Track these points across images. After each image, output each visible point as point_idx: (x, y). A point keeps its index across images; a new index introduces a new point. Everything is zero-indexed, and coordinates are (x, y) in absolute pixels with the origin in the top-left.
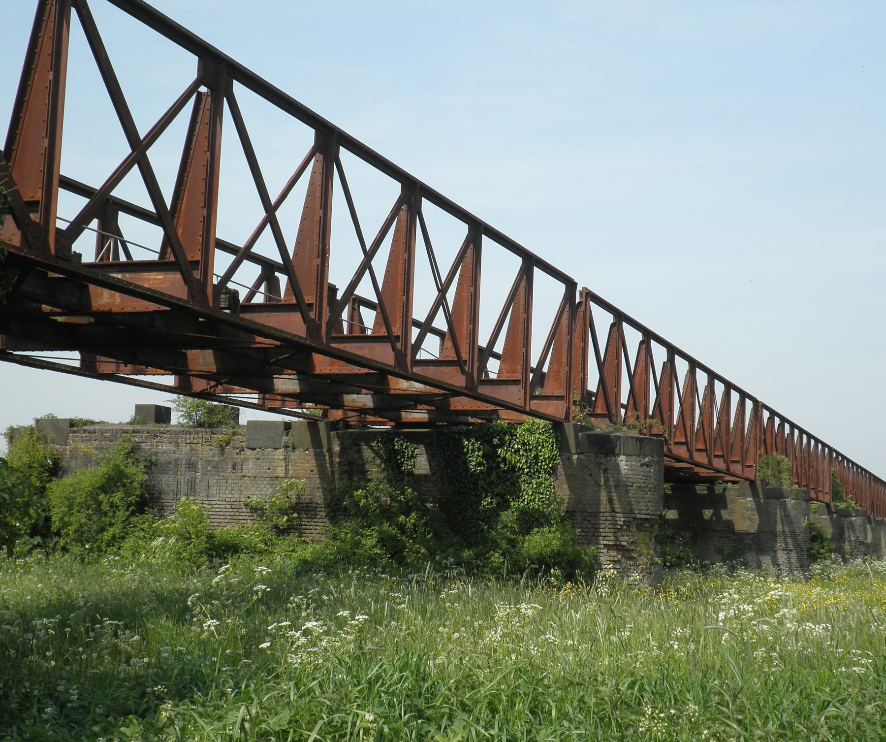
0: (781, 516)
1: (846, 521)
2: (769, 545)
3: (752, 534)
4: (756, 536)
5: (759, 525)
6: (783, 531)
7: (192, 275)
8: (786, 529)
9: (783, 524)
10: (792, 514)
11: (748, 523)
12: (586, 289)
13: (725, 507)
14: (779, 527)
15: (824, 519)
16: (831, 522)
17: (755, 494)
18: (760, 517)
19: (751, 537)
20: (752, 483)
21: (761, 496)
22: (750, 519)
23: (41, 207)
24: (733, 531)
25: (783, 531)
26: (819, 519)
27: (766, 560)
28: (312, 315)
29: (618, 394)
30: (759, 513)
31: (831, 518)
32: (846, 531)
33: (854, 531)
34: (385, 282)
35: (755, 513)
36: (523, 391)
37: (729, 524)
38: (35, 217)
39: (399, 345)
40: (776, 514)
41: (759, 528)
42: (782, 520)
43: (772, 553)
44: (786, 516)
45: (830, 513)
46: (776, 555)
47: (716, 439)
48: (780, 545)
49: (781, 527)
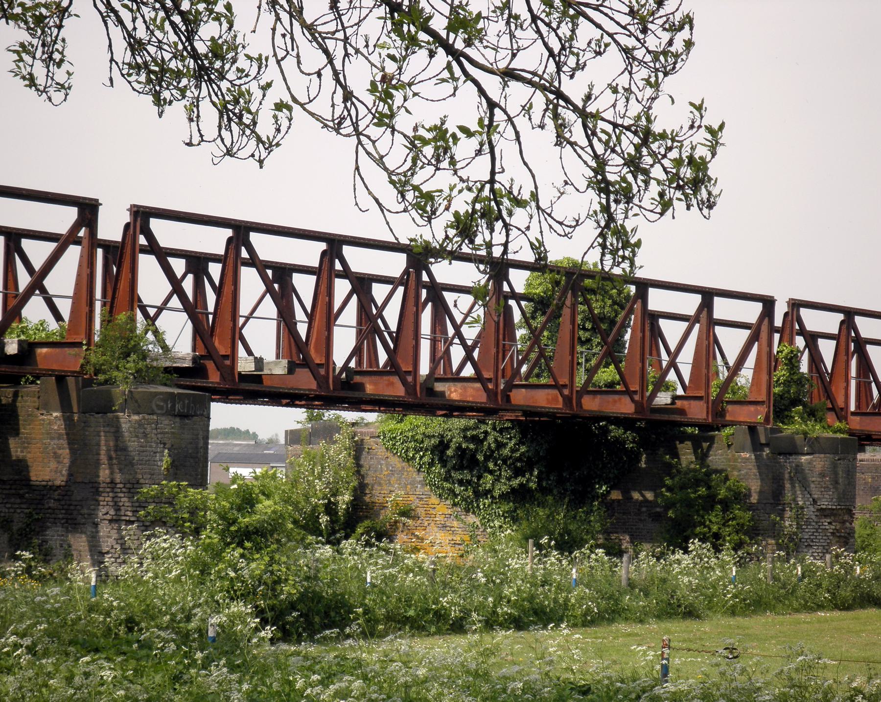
0: (108, 450)
1: (788, 464)
2: (85, 511)
3: (59, 487)
4: (65, 491)
5: (70, 467)
6: (112, 482)
7: (319, 373)
8: (118, 478)
9: (111, 466)
10: (133, 445)
11: (53, 465)
12: (135, 206)
13: (16, 433)
14: (104, 474)
15: (747, 460)
16: (759, 467)
17: (65, 406)
18: (73, 452)
19: (56, 495)
20: (61, 379)
21: (75, 409)
22: (56, 456)
23: (230, 358)
24: (25, 481)
25: (112, 482)
26: (735, 460)
27: (80, 542)
28: (490, 386)
29: (368, 343)
30: (70, 443)
31: (757, 458)
32: (788, 486)
33: (805, 486)
34: (690, 380)
35: (64, 442)
36: (705, 405)
37: (22, 467)
38: (228, 362)
39: (637, 397)
40: (98, 445)
41: (70, 475)
42: (110, 458)
43: (90, 529)
44: (120, 449)
45: (757, 446)
46: (97, 532)
47: (441, 358)
48: (104, 511)
49: (107, 472)
